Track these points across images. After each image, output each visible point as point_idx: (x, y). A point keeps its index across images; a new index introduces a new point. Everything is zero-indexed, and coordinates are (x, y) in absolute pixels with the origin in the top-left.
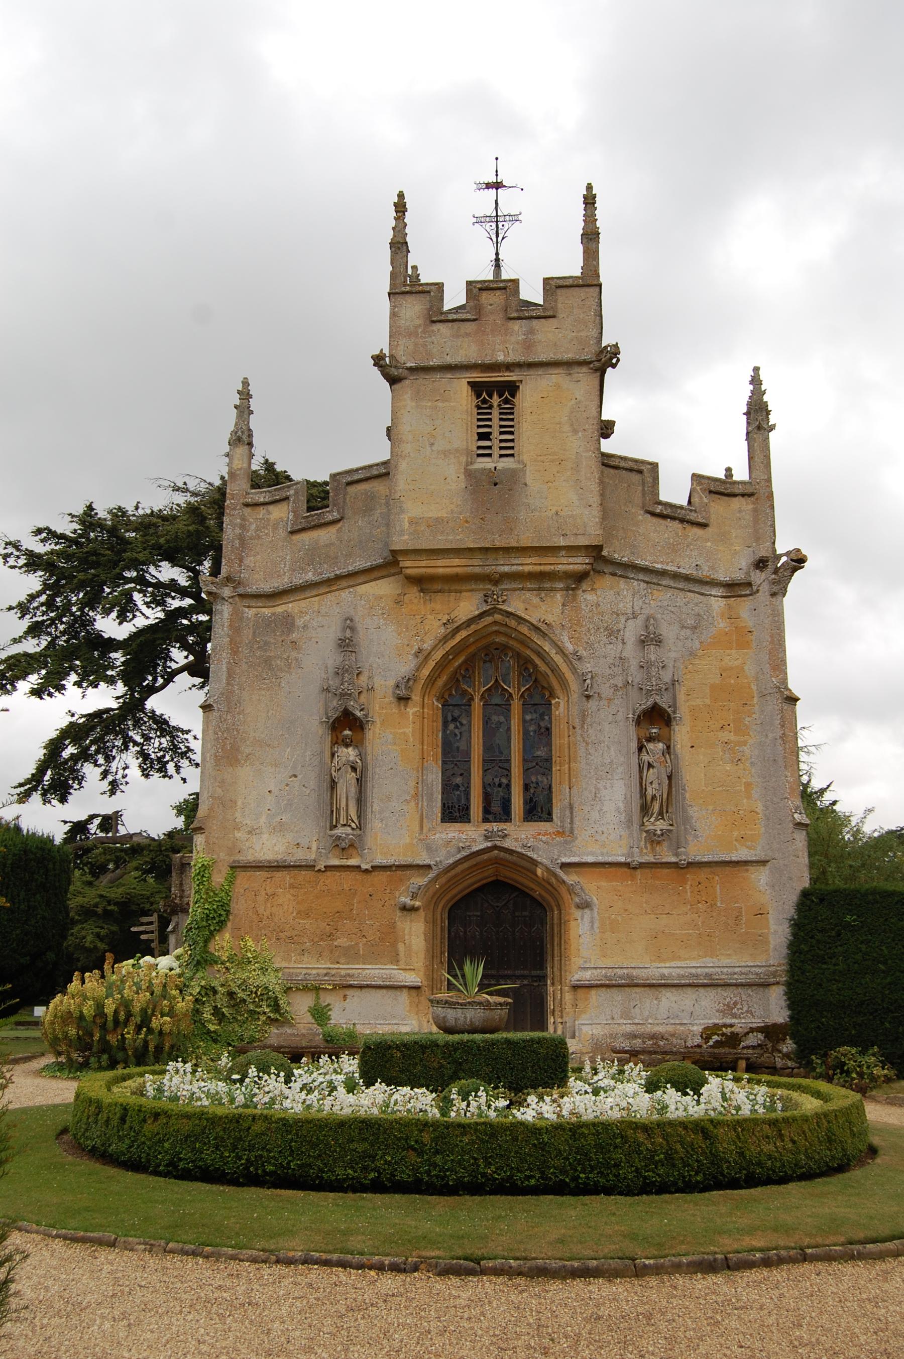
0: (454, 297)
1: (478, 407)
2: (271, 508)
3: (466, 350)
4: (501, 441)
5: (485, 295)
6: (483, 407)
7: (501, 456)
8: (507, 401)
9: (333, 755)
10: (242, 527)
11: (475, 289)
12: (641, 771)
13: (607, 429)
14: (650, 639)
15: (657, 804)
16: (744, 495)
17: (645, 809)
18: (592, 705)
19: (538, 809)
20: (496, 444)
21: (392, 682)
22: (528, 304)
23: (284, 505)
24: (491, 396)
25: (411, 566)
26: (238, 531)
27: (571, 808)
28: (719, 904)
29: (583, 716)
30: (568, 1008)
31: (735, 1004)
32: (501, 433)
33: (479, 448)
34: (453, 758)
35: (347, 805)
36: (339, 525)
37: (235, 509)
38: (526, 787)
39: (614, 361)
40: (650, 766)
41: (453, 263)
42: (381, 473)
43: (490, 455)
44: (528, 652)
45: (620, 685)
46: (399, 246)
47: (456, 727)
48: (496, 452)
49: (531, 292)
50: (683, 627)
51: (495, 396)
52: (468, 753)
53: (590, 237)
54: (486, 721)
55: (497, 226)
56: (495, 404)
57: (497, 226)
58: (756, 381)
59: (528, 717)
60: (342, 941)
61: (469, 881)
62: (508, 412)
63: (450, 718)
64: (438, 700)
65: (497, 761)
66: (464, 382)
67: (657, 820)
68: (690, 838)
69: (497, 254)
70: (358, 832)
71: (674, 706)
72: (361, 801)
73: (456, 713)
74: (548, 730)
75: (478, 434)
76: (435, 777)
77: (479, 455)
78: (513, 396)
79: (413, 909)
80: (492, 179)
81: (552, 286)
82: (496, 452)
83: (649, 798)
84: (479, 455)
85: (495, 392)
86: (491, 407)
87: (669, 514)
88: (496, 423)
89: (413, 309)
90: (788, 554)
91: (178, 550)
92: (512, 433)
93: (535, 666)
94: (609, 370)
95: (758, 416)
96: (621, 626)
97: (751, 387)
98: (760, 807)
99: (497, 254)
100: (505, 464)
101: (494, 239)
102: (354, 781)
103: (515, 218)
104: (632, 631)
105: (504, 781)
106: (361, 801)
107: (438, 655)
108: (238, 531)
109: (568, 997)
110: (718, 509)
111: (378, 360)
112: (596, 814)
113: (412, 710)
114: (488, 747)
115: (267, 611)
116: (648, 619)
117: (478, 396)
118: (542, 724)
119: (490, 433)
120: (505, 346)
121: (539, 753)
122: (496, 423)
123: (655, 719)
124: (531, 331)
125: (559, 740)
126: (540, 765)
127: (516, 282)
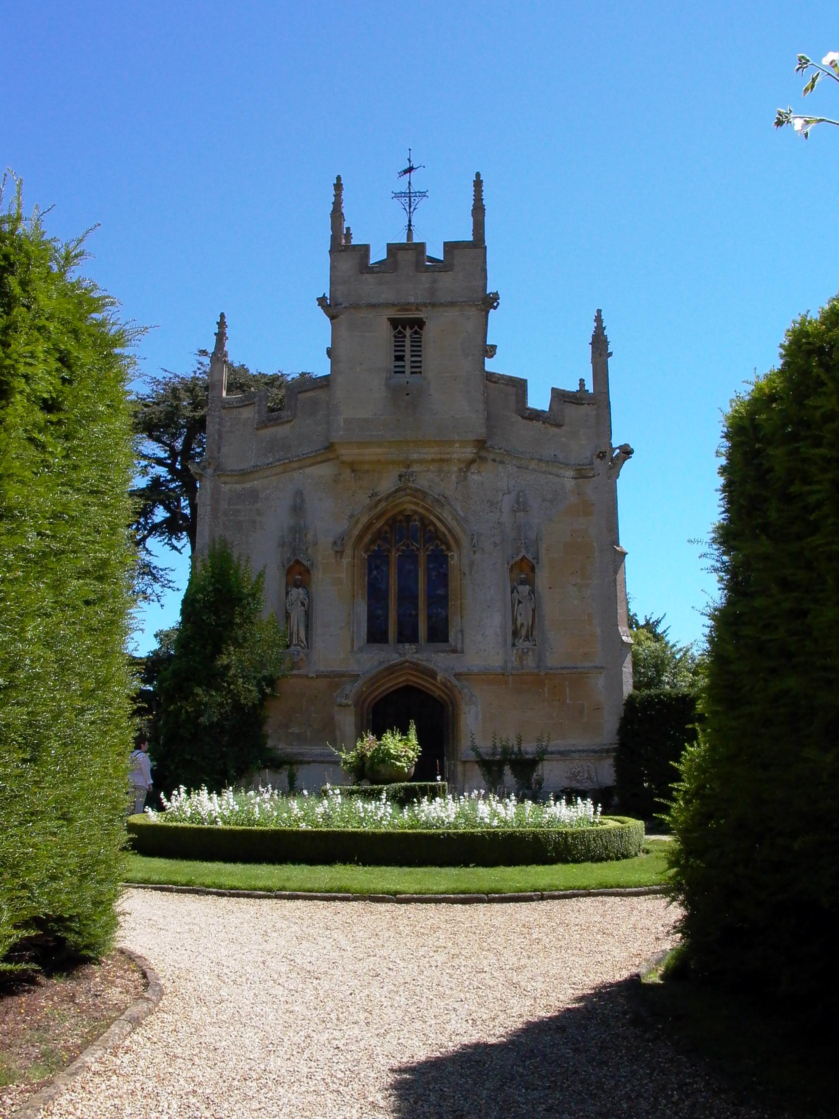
0: (378, 254)
1: (395, 337)
2: (241, 409)
3: (386, 295)
4: (412, 362)
5: (400, 253)
6: (399, 337)
7: (412, 373)
8: (416, 332)
9: (287, 593)
10: (220, 424)
11: (392, 249)
12: (513, 606)
13: (490, 351)
14: (520, 505)
15: (523, 633)
16: (587, 406)
17: (515, 634)
18: (478, 556)
19: (439, 633)
20: (408, 364)
21: (331, 540)
22: (431, 259)
23: (251, 408)
24: (405, 329)
25: (348, 453)
26: (217, 427)
27: (462, 631)
28: (568, 701)
29: (472, 564)
30: (460, 777)
31: (579, 772)
32: (412, 356)
33: (395, 367)
34: (376, 594)
35: (298, 631)
36: (292, 423)
37: (214, 411)
38: (429, 617)
39: (495, 304)
40: (520, 602)
41: (376, 233)
42: (325, 383)
43: (403, 372)
44: (432, 518)
45: (498, 542)
46: (337, 215)
47: (378, 573)
48: (408, 370)
49: (435, 251)
50: (544, 500)
51: (408, 329)
52: (387, 591)
53: (478, 210)
54: (400, 570)
55: (410, 200)
56: (408, 335)
57: (410, 200)
58: (599, 319)
59: (431, 566)
60: (295, 730)
61: (391, 684)
62: (417, 343)
63: (374, 566)
64: (365, 552)
65: (407, 596)
66: (385, 318)
67: (524, 641)
68: (547, 654)
69: (410, 221)
70: (305, 651)
71: (537, 558)
72: (308, 628)
73: (378, 562)
74: (446, 575)
75: (395, 356)
76: (362, 609)
77: (395, 372)
78: (421, 329)
79: (347, 706)
80: (407, 166)
81: (450, 247)
82: (408, 370)
83: (519, 625)
84: (395, 372)
85: (408, 327)
86: (405, 337)
87: (536, 415)
88: (408, 348)
89: (348, 264)
90: (620, 448)
91: (157, 427)
92: (420, 356)
93: (434, 525)
94: (492, 311)
95: (600, 345)
96: (500, 499)
97: (595, 324)
98: (598, 631)
99: (410, 221)
100: (413, 379)
101: (407, 208)
102: (303, 613)
103: (423, 195)
104: (507, 502)
105: (414, 613)
106: (308, 628)
107: (364, 520)
108: (217, 427)
109: (460, 769)
110: (572, 412)
111: (321, 301)
112: (482, 636)
113: (346, 560)
114: (401, 590)
115: (238, 487)
116: (518, 496)
117: (395, 328)
118: (441, 570)
119: (404, 356)
120: (412, 289)
121: (438, 592)
122: (408, 348)
123: (524, 571)
124: (434, 281)
125: (453, 584)
126: (440, 599)
127: (422, 245)
